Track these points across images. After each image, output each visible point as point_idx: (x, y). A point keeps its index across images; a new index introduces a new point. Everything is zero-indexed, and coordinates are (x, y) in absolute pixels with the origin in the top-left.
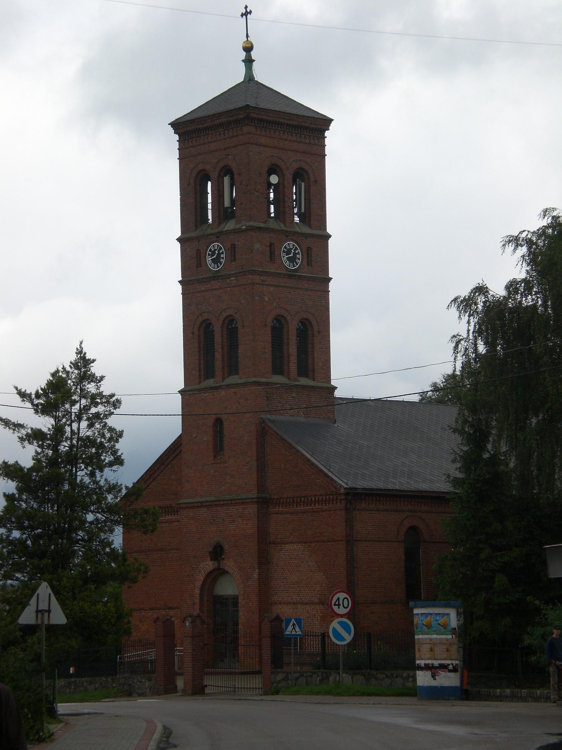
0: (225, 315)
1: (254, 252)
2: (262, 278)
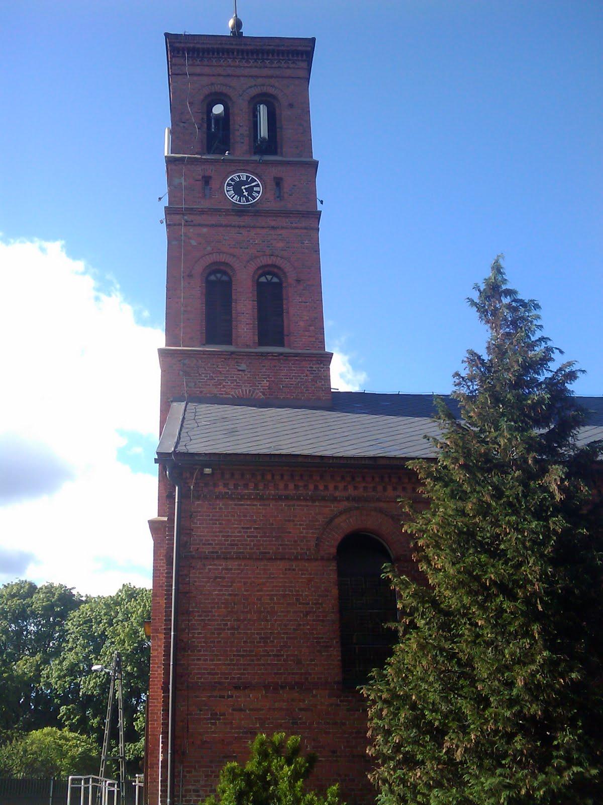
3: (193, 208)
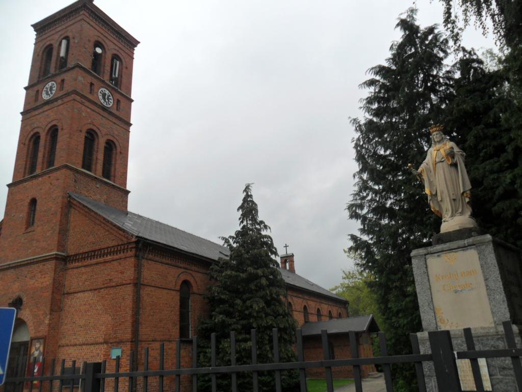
2: (82, 99)
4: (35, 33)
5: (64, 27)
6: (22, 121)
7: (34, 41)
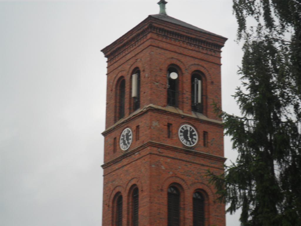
0: (130, 185)
1: (152, 128)
2: (159, 150)
3: (164, 145)
4: (106, 59)
5: (133, 54)
6: (104, 176)
7: (105, 71)
